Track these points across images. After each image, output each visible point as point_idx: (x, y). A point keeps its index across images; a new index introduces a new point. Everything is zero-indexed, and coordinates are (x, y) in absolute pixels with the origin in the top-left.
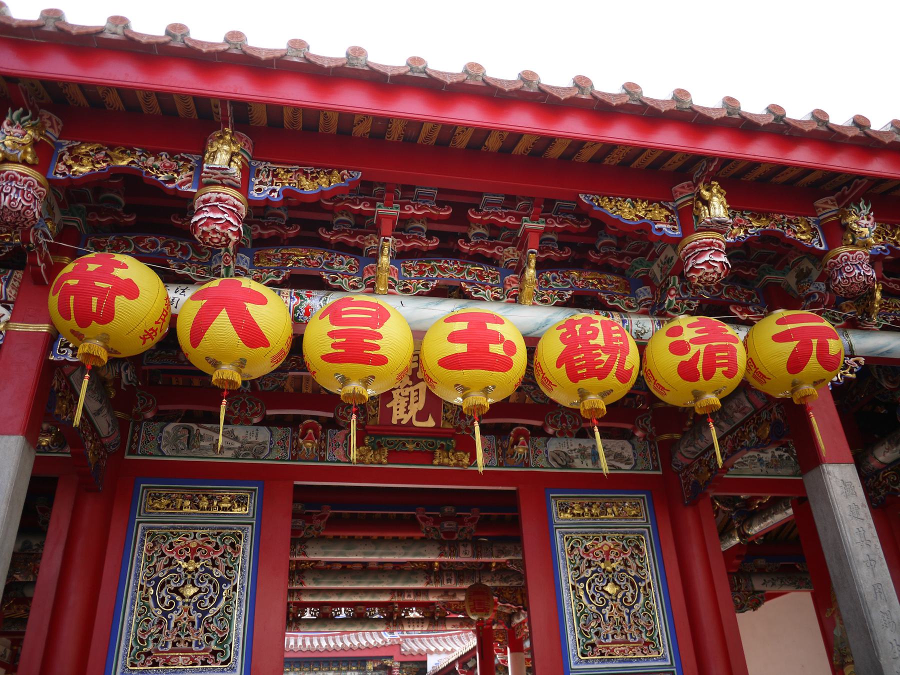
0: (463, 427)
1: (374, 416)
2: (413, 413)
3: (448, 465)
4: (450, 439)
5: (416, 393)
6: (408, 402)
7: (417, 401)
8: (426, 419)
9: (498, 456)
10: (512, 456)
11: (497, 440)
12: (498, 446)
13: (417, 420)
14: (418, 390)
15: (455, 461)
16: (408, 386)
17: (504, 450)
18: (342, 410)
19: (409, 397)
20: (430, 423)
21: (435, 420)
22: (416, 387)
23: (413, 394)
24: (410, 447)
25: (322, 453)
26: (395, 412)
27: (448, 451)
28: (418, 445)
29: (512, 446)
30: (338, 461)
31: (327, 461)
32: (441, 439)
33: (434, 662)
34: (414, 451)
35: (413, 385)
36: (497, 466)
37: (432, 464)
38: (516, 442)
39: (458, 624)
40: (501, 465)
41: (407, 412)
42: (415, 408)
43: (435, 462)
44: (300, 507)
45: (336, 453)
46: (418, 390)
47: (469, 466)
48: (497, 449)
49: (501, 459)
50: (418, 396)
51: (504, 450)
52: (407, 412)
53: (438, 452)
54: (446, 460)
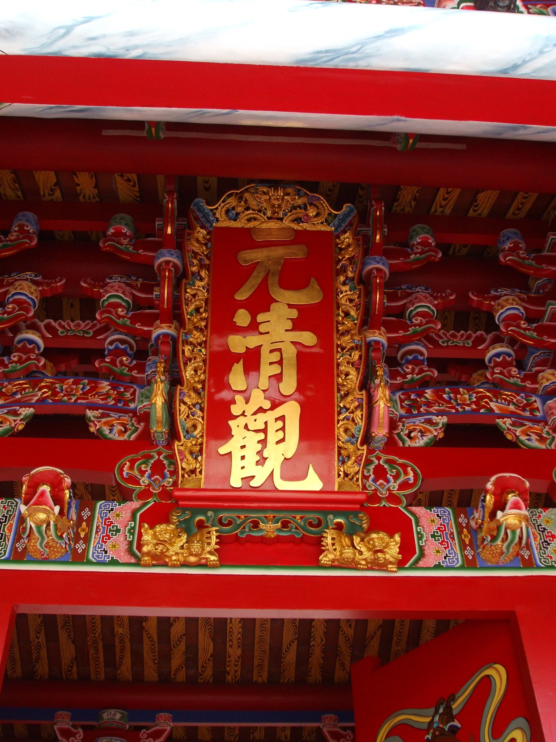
0: (383, 493)
1: (193, 471)
2: (274, 463)
3: (352, 565)
4: (355, 513)
5: (280, 424)
6: (263, 442)
7: (283, 440)
8: (303, 476)
9: (463, 546)
10: (494, 538)
11: (456, 517)
12: (459, 527)
13: (284, 477)
14: (282, 418)
15: (367, 554)
16: (261, 410)
17: (474, 532)
18: (131, 468)
19: (265, 431)
20: (312, 483)
21: (321, 477)
22: (278, 412)
23: (274, 426)
24: (270, 529)
25: (80, 547)
26: (236, 462)
27: (350, 536)
28: (285, 524)
29: (493, 515)
30: (114, 562)
31: (90, 563)
32: (337, 512)
33: (430, 738)
34: (278, 539)
35: (272, 408)
36: (462, 568)
37: (317, 565)
38: (500, 505)
39: (365, 375)
40: (470, 564)
41: (262, 461)
42: (276, 455)
43: (324, 559)
44: (118, 716)
45: (108, 545)
46: (282, 418)
47: (401, 564)
48: (460, 533)
49: (469, 552)
50: (283, 429)
51: (474, 532)
52: (262, 461)
53: (329, 538)
54: (348, 553)
